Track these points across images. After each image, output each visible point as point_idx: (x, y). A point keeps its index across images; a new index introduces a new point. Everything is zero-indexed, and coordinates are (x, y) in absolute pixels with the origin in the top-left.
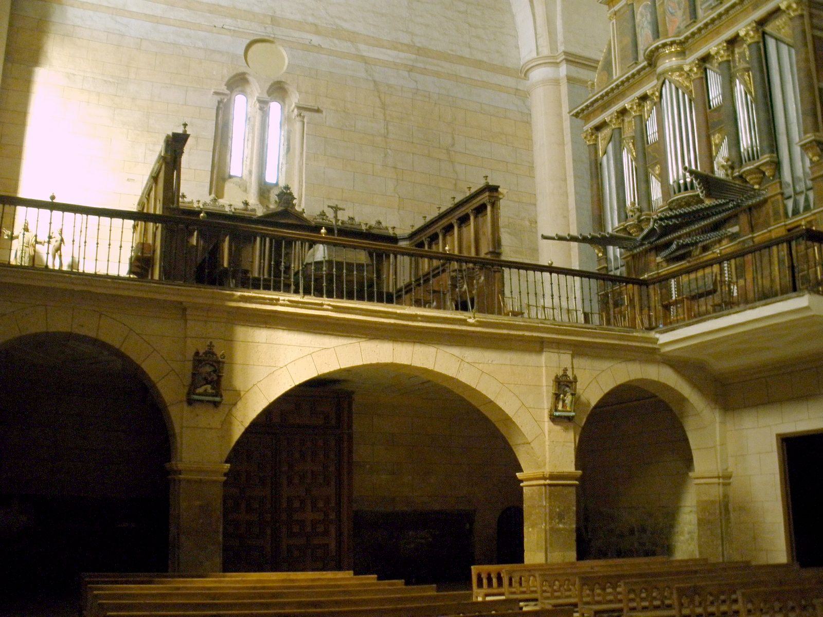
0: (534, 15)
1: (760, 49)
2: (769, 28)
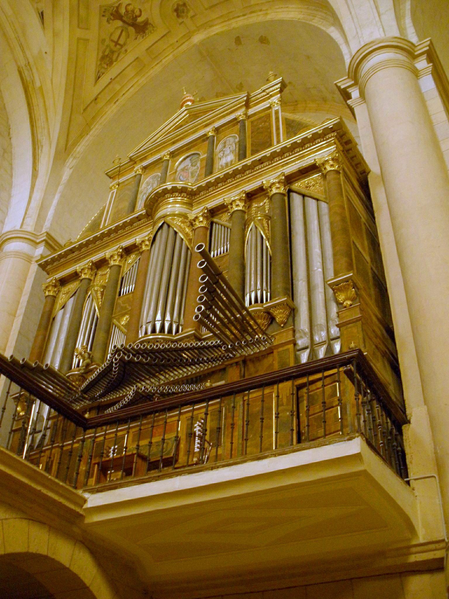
0: (30, 198)
1: (284, 201)
2: (296, 186)
